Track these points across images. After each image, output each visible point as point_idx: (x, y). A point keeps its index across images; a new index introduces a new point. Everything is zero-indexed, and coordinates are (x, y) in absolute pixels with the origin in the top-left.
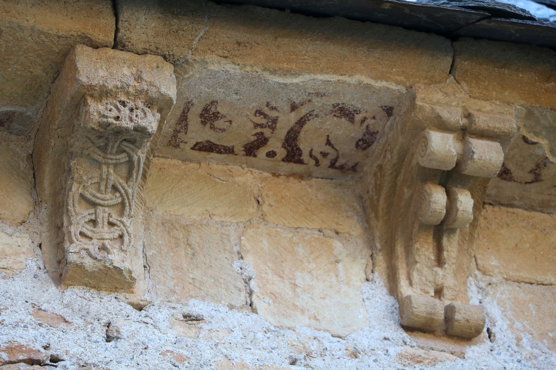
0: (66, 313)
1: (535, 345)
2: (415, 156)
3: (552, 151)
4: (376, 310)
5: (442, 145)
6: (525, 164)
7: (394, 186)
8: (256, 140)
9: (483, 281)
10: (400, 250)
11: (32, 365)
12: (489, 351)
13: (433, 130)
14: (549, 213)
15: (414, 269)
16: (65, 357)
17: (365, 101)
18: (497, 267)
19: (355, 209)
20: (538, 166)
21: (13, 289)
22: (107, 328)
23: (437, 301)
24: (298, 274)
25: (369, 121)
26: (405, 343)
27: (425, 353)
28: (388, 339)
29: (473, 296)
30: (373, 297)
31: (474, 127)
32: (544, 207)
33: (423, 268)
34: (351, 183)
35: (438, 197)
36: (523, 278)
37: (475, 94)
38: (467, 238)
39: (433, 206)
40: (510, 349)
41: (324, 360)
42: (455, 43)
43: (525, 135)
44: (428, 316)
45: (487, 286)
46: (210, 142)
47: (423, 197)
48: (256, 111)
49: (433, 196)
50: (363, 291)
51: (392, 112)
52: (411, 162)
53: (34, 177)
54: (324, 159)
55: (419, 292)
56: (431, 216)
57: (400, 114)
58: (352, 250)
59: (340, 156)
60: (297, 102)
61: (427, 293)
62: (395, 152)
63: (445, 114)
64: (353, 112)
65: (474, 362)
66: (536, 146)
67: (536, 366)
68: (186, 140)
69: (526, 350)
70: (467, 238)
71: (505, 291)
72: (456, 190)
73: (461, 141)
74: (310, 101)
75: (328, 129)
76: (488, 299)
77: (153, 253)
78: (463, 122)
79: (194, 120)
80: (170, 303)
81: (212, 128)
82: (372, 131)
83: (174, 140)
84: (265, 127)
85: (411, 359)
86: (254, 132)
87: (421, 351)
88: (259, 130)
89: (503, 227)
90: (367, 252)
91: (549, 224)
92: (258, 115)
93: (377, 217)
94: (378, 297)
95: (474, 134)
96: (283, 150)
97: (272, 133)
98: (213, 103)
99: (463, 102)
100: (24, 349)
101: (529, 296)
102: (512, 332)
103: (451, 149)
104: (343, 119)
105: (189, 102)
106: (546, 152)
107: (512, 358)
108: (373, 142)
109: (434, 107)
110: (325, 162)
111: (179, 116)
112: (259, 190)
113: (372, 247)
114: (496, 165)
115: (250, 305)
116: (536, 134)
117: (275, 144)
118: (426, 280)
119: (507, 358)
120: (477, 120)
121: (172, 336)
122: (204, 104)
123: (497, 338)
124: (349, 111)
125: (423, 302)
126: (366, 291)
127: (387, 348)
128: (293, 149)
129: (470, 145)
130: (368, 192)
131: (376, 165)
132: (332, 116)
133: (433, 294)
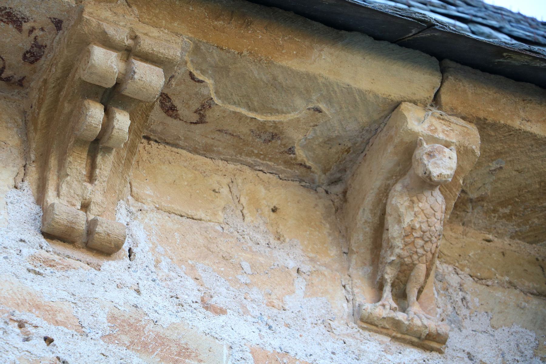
1: (172, 268)
2: (78, 71)
3: (217, 92)
4: (18, 214)
5: (104, 62)
6: (190, 103)
7: (56, 101)
9: (133, 206)
10: (53, 162)
12: (127, 268)
13: (98, 46)
14: (211, 158)
15: (63, 182)
17: (34, 9)
18: (150, 196)
20: (203, 106)
23: (82, 213)
25: (38, 33)
26: (42, 248)
27: (60, 259)
28: (24, 241)
29: (121, 217)
30: (17, 202)
31: (138, 48)
32: (206, 151)
33: (73, 181)
34: (17, 98)
35: (95, 113)
36: (174, 210)
37: (145, 19)
38: (123, 162)
39: (89, 120)
40: (147, 269)
43: (192, 71)
44: (69, 225)
45: (137, 211)
47: (81, 112)
49: (90, 110)
50: (8, 196)
52: (74, 77)
55: (65, 203)
56: (86, 130)
57: (68, 28)
58: (4, 157)
59: (7, 67)
61: (74, 205)
62: (59, 65)
63: (111, 31)
64: (21, 20)
65: (109, 274)
66: (202, 84)
67: (170, 286)
69: (163, 272)
70: (123, 162)
71: (154, 219)
72: (116, 110)
73: (126, 61)
76: (136, 222)
78: (129, 42)
85: (44, 262)
87: (56, 256)
89: (164, 163)
90: (20, 162)
91: (209, 168)
93: (35, 130)
94: (24, 203)
95: (139, 57)
99: (131, 24)
101: (176, 226)
103: (113, 65)
104: (10, 26)
106: (211, 92)
108: (41, 56)
109: (101, 23)
113: (25, 155)
114: (155, 89)
116: (203, 72)
118: (75, 193)
119: (143, 276)
120: (142, 43)
123: (136, 258)
124: (17, 18)
125: (64, 207)
126: (12, 195)
127: (21, 248)
129: (133, 66)
130: (31, 107)
131: (42, 80)
133: (79, 208)
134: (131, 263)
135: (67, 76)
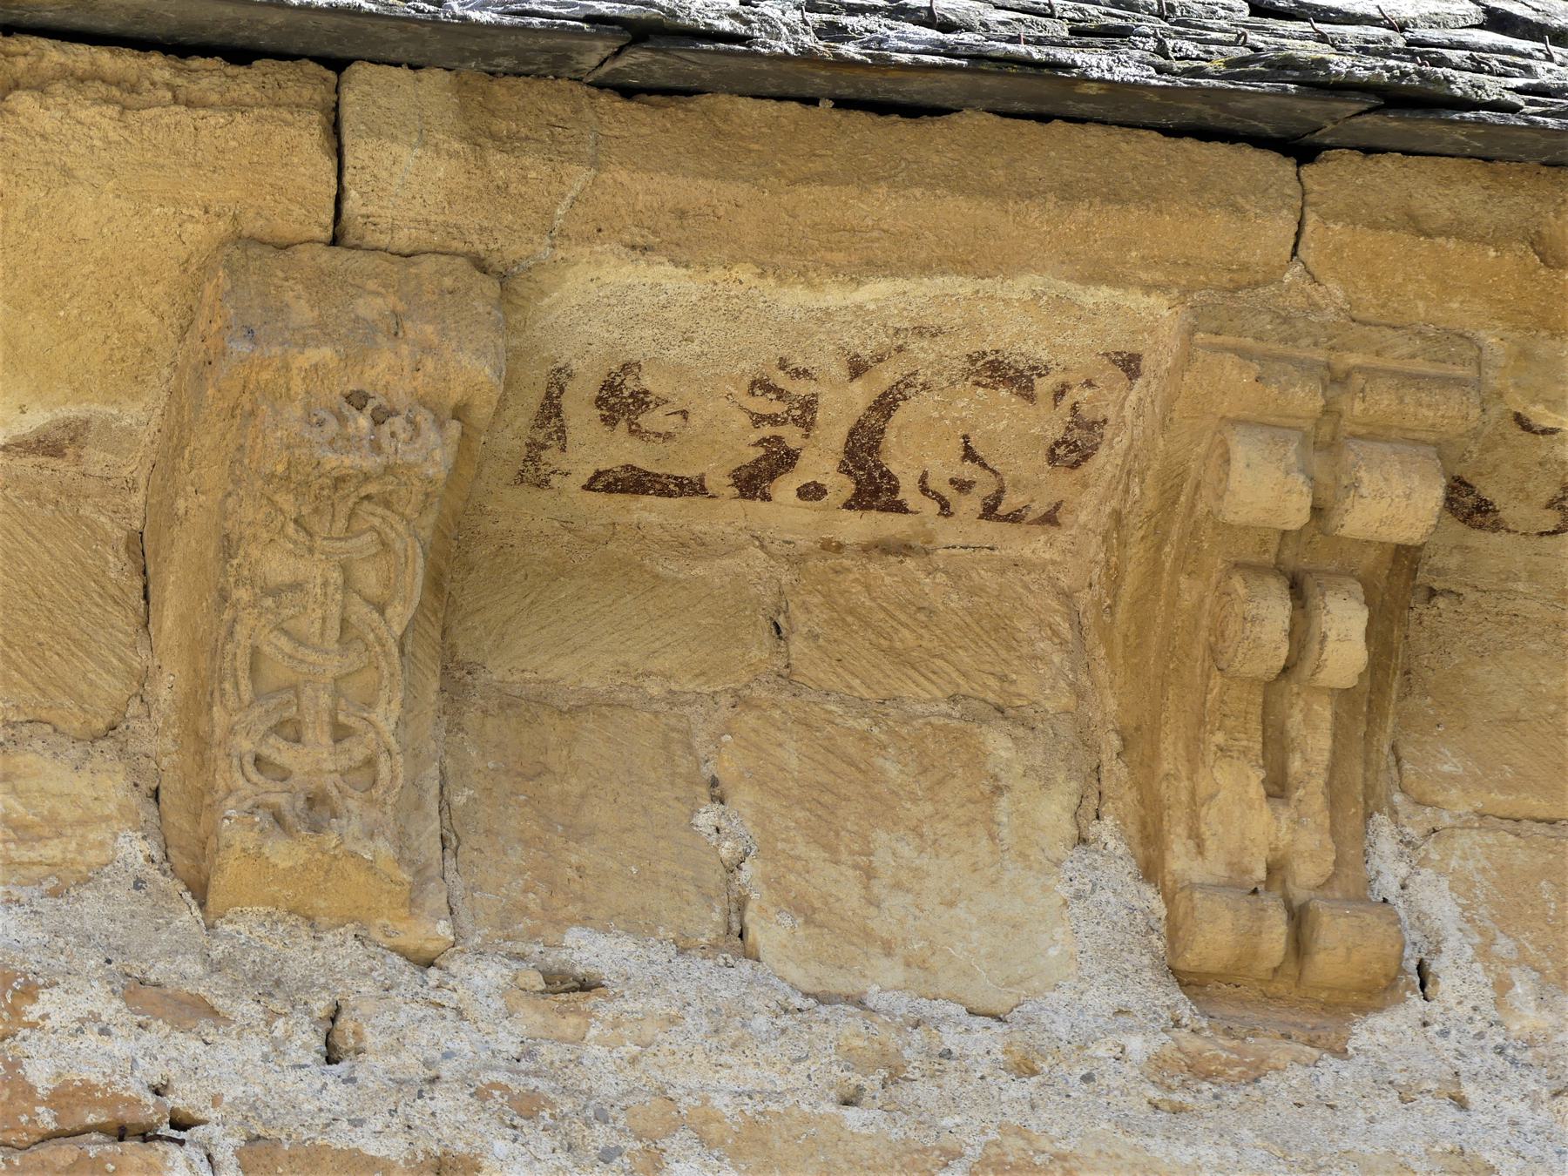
0: (213, 991)
6: (1530, 486)
8: (765, 458)
11: (121, 1139)
16: (212, 1114)
19: (1055, 633)
21: (76, 924)
22: (329, 1025)
24: (881, 837)
25: (1079, 394)
41: (939, 1087)
42: (1307, 170)
46: (634, 468)
48: (754, 383)
51: (1138, 366)
53: (146, 597)
54: (962, 497)
59: (1009, 489)
60: (865, 354)
68: (566, 467)
71: (1472, 851)
74: (900, 349)
75: (963, 420)
76: (1427, 873)
77: (468, 797)
79: (580, 415)
80: (509, 944)
81: (635, 431)
82: (1088, 418)
83: (532, 469)
84: (785, 422)
86: (755, 436)
88: (767, 431)
92: (759, 392)
96: (844, 478)
97: (807, 436)
98: (626, 368)
100: (99, 1094)
102: (1487, 969)
104: (1003, 392)
105: (559, 370)
107: (1482, 1042)
108: (1095, 448)
110: (969, 505)
111: (536, 408)
112: (781, 593)
115: (741, 936)
117: (821, 461)
121: (511, 1039)
122: (604, 373)
128: (870, 474)
132: (968, 384)
134: (1428, 1005)
135: (1174, 503)
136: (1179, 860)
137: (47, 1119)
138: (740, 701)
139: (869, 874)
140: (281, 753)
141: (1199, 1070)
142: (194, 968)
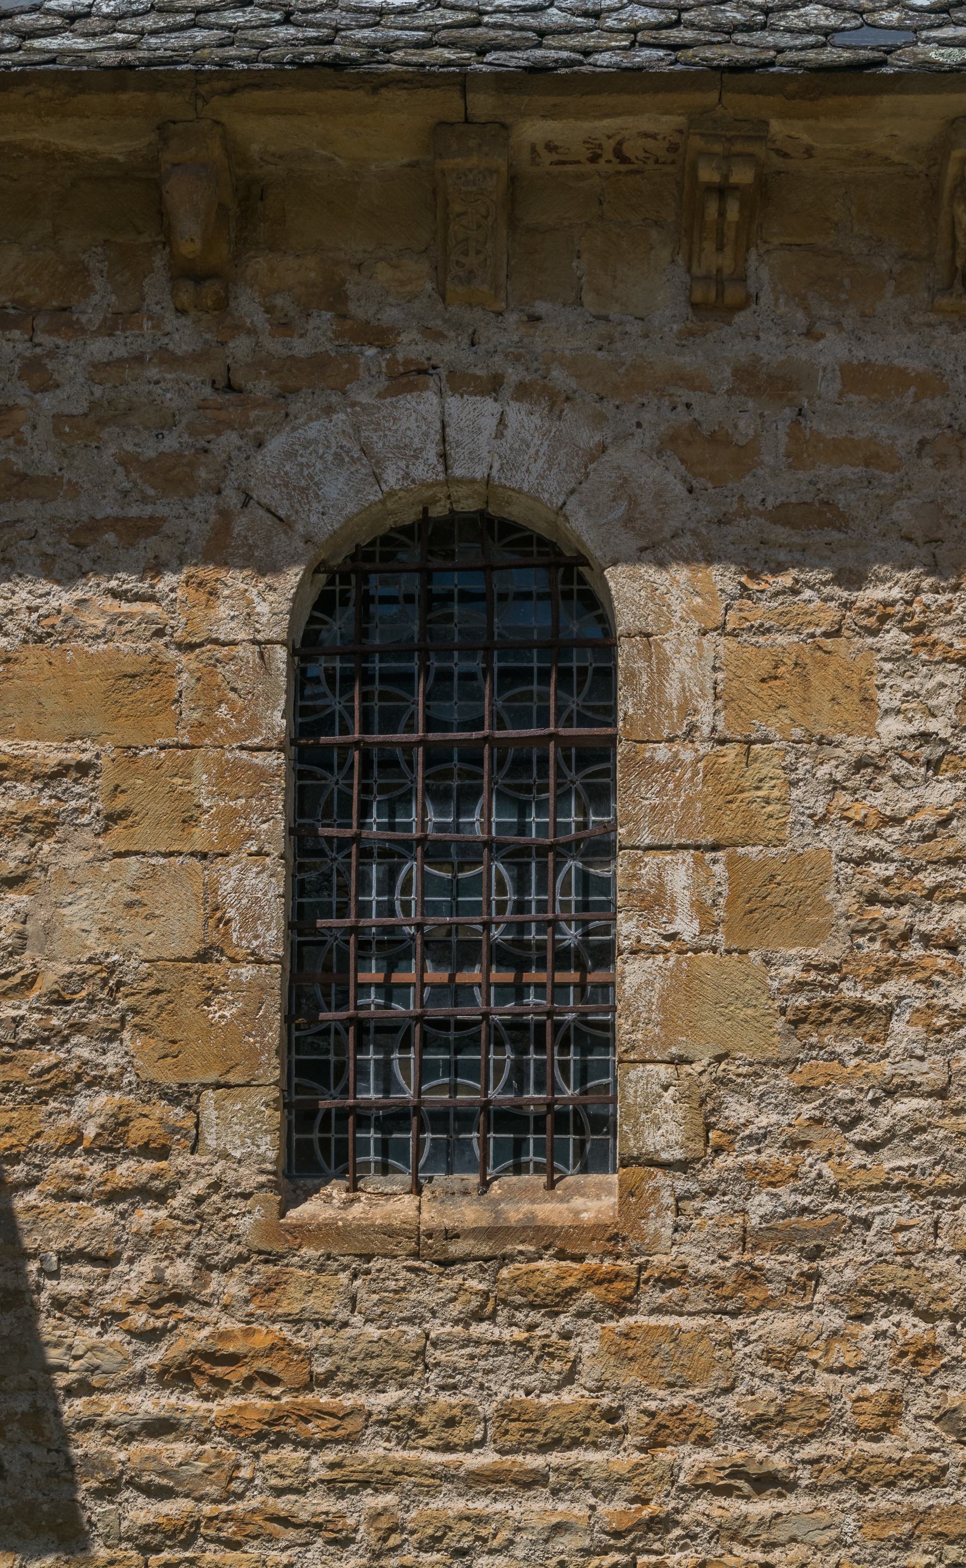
136: (695, 269)
137: (401, 369)
138: (589, 225)
139: (615, 278)
140: (463, 260)
141: (692, 334)
142: (439, 322)
